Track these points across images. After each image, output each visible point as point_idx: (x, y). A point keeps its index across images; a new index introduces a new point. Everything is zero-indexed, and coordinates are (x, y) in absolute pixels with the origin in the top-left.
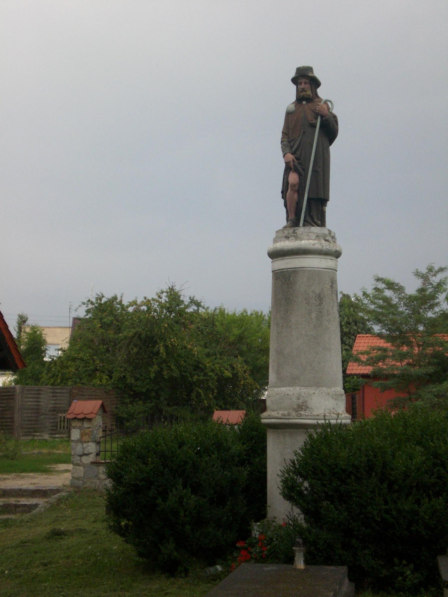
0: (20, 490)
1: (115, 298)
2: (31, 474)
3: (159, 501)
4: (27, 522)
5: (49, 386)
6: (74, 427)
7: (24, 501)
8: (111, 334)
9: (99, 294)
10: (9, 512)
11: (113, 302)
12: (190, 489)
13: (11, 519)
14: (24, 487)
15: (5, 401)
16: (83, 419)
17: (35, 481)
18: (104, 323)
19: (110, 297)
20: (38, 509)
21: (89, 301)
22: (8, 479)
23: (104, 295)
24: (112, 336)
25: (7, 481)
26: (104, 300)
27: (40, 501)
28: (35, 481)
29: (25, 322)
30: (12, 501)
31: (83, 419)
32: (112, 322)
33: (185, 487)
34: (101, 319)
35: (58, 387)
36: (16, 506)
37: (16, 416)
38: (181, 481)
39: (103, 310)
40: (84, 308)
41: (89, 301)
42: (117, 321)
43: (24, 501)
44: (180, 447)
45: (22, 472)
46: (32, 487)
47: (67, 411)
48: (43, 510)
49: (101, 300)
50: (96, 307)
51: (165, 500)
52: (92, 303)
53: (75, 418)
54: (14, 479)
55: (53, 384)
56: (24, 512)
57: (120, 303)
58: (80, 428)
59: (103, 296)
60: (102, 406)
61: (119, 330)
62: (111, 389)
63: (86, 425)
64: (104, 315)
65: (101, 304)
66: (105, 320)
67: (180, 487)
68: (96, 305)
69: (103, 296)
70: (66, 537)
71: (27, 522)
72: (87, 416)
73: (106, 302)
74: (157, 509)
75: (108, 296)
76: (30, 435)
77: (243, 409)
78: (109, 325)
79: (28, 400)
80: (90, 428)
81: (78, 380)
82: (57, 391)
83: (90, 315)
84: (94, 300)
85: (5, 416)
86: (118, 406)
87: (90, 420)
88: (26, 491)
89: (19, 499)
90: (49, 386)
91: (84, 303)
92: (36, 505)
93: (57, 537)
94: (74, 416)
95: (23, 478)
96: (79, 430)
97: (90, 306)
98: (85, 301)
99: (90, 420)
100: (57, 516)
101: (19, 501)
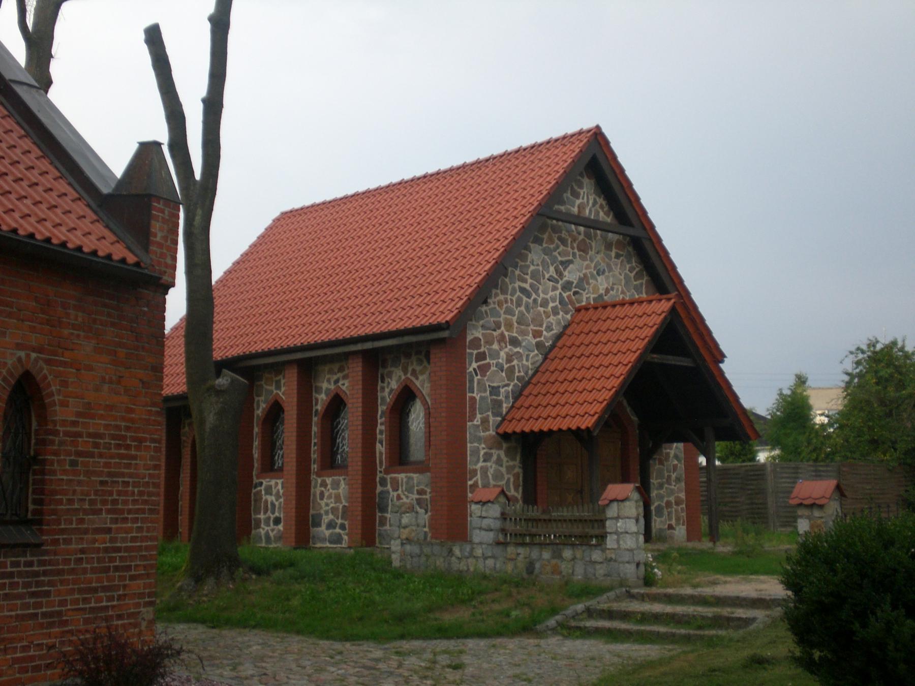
0: (738, 597)
1: (894, 343)
2: (762, 577)
3: (857, 626)
4: (738, 641)
5: (811, 463)
6: (801, 517)
7: (740, 613)
8: (891, 392)
9: (871, 338)
10: (720, 627)
11: (892, 348)
12: (903, 610)
13: (717, 636)
14: (743, 594)
15: (755, 482)
16: (812, 506)
17: (763, 586)
18: (881, 377)
19: (887, 343)
20: (755, 625)
21: (858, 349)
22: (730, 582)
23: (879, 339)
24: (892, 394)
25: (728, 586)
26: (879, 347)
27: (759, 614)
28: (763, 586)
29: (804, 382)
30: (726, 611)
31: (812, 506)
32: (891, 376)
33: (894, 607)
34: (876, 372)
35: (822, 464)
36: (729, 619)
37: (770, 500)
38: (888, 598)
39: (879, 360)
40: (852, 358)
41: (858, 349)
42: (900, 373)
43: (740, 613)
44: (886, 547)
45: (752, 574)
46: (754, 595)
47: (791, 492)
48: (761, 626)
49: (874, 346)
50: (869, 357)
51: (864, 626)
52: (863, 352)
53: (801, 505)
54: (738, 582)
55: (816, 460)
56: (738, 627)
57: (902, 349)
58: (808, 518)
59: (877, 342)
60: (838, 487)
61: (901, 385)
62: (896, 464)
63: (817, 513)
64: (880, 367)
65: (875, 353)
66: (881, 374)
67: (887, 607)
68: (869, 353)
69: (877, 342)
70: (771, 667)
71: (738, 641)
72: (817, 502)
73: (882, 350)
74: (855, 638)
75: (884, 340)
76: (790, 526)
77: (635, 482)
78: (887, 380)
79: (784, 480)
80: (822, 518)
81: (849, 454)
82: (821, 469)
83: (861, 368)
84: (864, 347)
85: (756, 501)
86: (908, 488)
87: (821, 507)
88: (745, 599)
89: (734, 610)
90: (811, 463)
91: (851, 353)
92: (754, 619)
93: (757, 665)
94: (800, 501)
95: (750, 581)
96: (807, 521)
97: (860, 356)
98: (853, 349)
99: (821, 507)
100: (777, 636)
101: (733, 613)
